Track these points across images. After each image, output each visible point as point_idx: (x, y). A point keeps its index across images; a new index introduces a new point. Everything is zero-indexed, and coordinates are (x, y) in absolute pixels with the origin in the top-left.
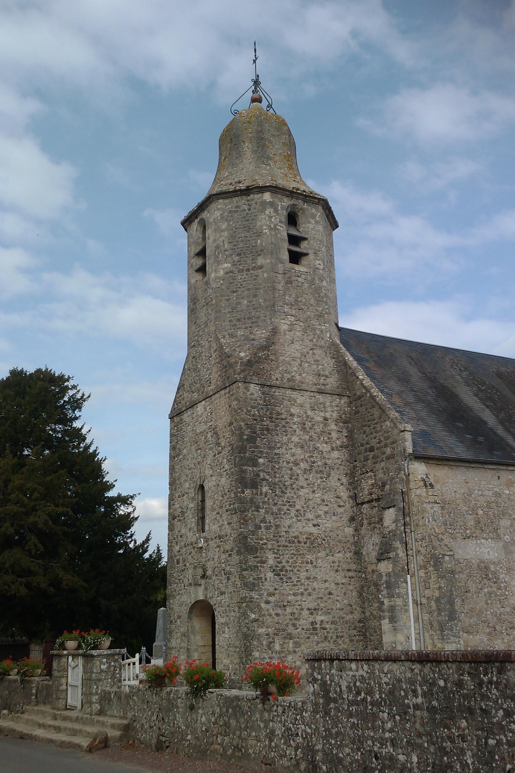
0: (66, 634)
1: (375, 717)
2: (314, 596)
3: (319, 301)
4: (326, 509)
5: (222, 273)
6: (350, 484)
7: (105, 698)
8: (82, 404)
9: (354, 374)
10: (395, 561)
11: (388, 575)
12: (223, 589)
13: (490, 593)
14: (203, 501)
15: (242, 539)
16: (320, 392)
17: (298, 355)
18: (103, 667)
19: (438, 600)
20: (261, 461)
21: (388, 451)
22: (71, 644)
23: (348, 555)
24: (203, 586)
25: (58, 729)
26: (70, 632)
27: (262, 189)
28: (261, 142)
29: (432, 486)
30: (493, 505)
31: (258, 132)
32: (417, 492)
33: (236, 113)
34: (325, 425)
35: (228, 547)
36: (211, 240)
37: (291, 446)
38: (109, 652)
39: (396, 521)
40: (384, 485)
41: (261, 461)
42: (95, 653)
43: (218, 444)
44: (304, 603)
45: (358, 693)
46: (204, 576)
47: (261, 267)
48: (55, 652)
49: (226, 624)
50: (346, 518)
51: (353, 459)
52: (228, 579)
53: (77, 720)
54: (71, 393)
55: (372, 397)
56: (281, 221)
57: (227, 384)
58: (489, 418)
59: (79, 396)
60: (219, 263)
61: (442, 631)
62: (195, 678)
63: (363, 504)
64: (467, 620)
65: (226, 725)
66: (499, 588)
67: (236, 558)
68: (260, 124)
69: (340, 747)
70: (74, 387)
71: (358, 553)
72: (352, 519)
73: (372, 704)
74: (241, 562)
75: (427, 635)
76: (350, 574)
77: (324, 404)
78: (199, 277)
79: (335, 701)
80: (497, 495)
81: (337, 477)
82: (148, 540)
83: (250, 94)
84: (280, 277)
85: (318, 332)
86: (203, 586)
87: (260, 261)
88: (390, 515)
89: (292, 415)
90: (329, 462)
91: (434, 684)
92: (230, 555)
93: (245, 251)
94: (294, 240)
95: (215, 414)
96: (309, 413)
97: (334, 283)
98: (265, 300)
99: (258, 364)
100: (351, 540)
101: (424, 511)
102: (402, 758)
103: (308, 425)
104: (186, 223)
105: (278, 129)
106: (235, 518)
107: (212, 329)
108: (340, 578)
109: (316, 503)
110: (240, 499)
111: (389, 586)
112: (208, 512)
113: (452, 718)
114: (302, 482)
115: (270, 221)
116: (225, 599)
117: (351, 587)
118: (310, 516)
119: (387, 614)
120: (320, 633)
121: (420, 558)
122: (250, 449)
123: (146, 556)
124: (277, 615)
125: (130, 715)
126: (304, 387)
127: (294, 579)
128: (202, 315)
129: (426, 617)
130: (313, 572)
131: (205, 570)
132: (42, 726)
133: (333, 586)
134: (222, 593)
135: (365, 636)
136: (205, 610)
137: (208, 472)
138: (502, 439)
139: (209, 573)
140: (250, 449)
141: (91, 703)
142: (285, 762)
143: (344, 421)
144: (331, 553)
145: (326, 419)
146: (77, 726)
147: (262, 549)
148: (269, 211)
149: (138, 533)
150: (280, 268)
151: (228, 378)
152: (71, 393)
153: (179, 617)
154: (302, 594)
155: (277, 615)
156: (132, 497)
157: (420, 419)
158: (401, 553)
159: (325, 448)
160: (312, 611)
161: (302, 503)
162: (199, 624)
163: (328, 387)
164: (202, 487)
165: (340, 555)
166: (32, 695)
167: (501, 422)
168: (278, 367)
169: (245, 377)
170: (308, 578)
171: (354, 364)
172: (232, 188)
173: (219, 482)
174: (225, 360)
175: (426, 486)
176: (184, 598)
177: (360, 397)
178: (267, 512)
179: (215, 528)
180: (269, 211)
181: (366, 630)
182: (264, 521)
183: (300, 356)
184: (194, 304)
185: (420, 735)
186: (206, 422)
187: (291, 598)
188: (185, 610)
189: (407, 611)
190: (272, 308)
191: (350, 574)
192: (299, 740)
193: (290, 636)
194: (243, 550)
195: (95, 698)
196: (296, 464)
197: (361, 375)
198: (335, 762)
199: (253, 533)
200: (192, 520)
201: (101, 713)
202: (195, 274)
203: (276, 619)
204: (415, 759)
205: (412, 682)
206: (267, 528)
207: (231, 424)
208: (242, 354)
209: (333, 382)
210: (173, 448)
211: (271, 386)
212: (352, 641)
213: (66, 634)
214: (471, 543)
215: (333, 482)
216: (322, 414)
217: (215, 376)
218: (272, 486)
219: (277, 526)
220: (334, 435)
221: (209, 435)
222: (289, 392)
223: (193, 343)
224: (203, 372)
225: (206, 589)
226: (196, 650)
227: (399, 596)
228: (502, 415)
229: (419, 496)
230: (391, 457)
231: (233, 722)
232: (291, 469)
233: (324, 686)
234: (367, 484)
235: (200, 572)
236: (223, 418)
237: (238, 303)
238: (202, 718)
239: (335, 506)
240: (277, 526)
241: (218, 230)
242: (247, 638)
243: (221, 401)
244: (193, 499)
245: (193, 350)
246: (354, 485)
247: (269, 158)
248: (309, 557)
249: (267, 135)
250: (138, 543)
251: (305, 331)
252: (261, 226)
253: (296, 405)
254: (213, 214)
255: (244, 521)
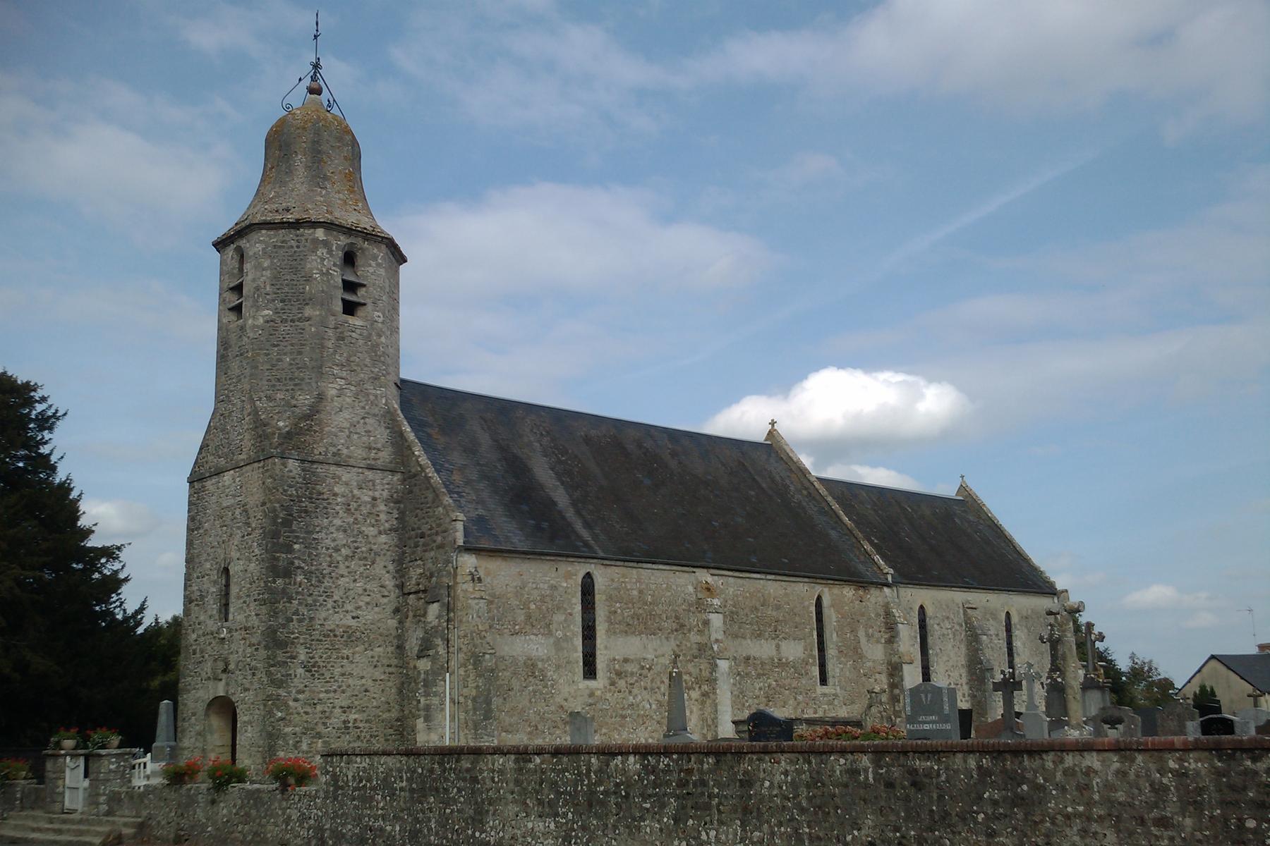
0: (62, 732)
1: (372, 798)
2: (348, 694)
3: (376, 360)
4: (367, 599)
5: (261, 320)
6: (397, 572)
7: (115, 799)
8: (53, 423)
9: (409, 447)
10: (434, 659)
11: (426, 673)
12: (247, 686)
13: (535, 692)
14: (227, 585)
15: (271, 633)
16: (370, 468)
17: (346, 425)
18: (112, 767)
19: (474, 700)
20: (296, 547)
21: (439, 539)
22: (69, 743)
23: (390, 649)
24: (223, 682)
25: (59, 832)
26: (67, 730)
27: (314, 225)
28: (317, 156)
29: (480, 580)
30: (548, 599)
31: (314, 142)
32: (464, 587)
33: (288, 107)
34: (374, 506)
35: (254, 641)
36: (250, 277)
37: (332, 529)
38: (119, 751)
39: (439, 617)
40: (432, 575)
41: (296, 547)
42: (103, 752)
43: (248, 524)
44: (342, 696)
45: (361, 781)
46: (225, 671)
47: (308, 319)
48: (50, 752)
49: (250, 722)
50: (389, 609)
51: (402, 544)
52: (254, 674)
53: (80, 822)
54: (39, 408)
55: (428, 478)
56: (335, 265)
57: (262, 456)
58: (561, 498)
59: (50, 413)
60: (258, 309)
61: (476, 730)
62: (218, 774)
63: (409, 594)
64: (507, 719)
65: (247, 815)
66: (546, 686)
67: (263, 653)
68: (317, 133)
69: (343, 825)
70: (43, 399)
71: (400, 648)
72: (397, 611)
73: (371, 789)
74: (268, 658)
75: (462, 734)
76: (390, 670)
77: (373, 481)
78: (232, 317)
79: (342, 788)
80: (554, 588)
81: (383, 564)
82: (142, 609)
83: (307, 82)
84: (330, 333)
85: (372, 398)
86: (223, 682)
87: (308, 311)
88: (434, 609)
89: (335, 495)
90: (374, 547)
91: (415, 771)
92: (257, 649)
93: (291, 297)
94: (350, 287)
95: (243, 488)
96: (356, 492)
97: (398, 333)
98: (311, 359)
99: (298, 438)
100: (394, 633)
101: (469, 607)
102: (389, 828)
103: (353, 505)
104: (220, 245)
105: (340, 139)
106: (264, 610)
107: (247, 387)
108: (378, 674)
109: (357, 594)
110: (270, 588)
111: (427, 684)
112: (232, 599)
113: (425, 796)
114: (342, 570)
115: (323, 265)
116: (249, 696)
117: (390, 684)
118: (349, 607)
119: (422, 713)
120: (354, 732)
121: (461, 655)
122: (286, 533)
123: (140, 630)
124: (306, 713)
125: (145, 813)
126: (352, 462)
127: (328, 675)
128: (235, 366)
129: (462, 715)
130: (348, 669)
131: (227, 664)
132: (39, 830)
133: (370, 683)
134: (246, 690)
135: (401, 734)
136: (225, 708)
137: (235, 555)
138: (569, 525)
139: (232, 667)
140: (286, 533)
141: (98, 804)
142: (299, 841)
143: (396, 501)
144: (370, 647)
145: (374, 499)
146: (82, 827)
147: (293, 643)
148: (322, 251)
149: (129, 598)
150: (332, 321)
151: (263, 450)
152: (39, 408)
153: (194, 714)
154: (335, 691)
155: (306, 713)
156: (119, 548)
157: (480, 502)
158: (442, 651)
159: (371, 531)
160: (345, 710)
161: (341, 593)
162: (216, 722)
163: (379, 462)
164: (226, 570)
165: (381, 649)
166: (16, 799)
167: (574, 504)
168: (322, 439)
169: (283, 452)
170: (343, 675)
171: (411, 436)
172: (278, 218)
173: (247, 567)
174: (260, 427)
175: (473, 580)
176: (201, 693)
177: (415, 476)
178: (300, 604)
179: (240, 618)
180: (322, 251)
181: (402, 728)
182: (297, 613)
183: (353, 424)
184: (226, 349)
185: (402, 811)
186: (234, 496)
187: (322, 695)
188: (201, 707)
189: (443, 710)
190: (319, 370)
191: (390, 670)
192: (312, 822)
193: (319, 735)
194: (271, 645)
195: (102, 799)
196: (337, 550)
197: (418, 450)
198: (338, 836)
199: (284, 626)
200: (213, 607)
201: (108, 814)
202: (228, 313)
203: (305, 717)
204: (398, 828)
205: (400, 770)
206: (300, 621)
207: (264, 504)
208: (281, 424)
209: (385, 456)
210: (191, 519)
211: (313, 462)
212: (387, 740)
213: (62, 732)
214: (519, 640)
215: (378, 569)
216: (370, 493)
217: (246, 442)
218: (308, 575)
219: (312, 619)
220: (383, 517)
221: (238, 511)
222: (333, 468)
223: (221, 397)
224: (233, 436)
225: (227, 684)
226: (213, 750)
227: (436, 694)
228: (577, 494)
229: (465, 591)
230: (441, 546)
231: (253, 812)
232: (331, 556)
233: (335, 778)
234: (415, 573)
235: (221, 665)
236: (254, 496)
237: (280, 360)
238: (223, 810)
239: (379, 596)
240: (312, 619)
241: (258, 267)
242: (272, 738)
243: (253, 475)
244: (215, 582)
245: (222, 407)
246: (401, 573)
247: (325, 178)
248: (345, 652)
249: (324, 147)
250: (130, 611)
251: (356, 396)
252: (312, 269)
253: (342, 483)
254: (255, 245)
255: (274, 614)
